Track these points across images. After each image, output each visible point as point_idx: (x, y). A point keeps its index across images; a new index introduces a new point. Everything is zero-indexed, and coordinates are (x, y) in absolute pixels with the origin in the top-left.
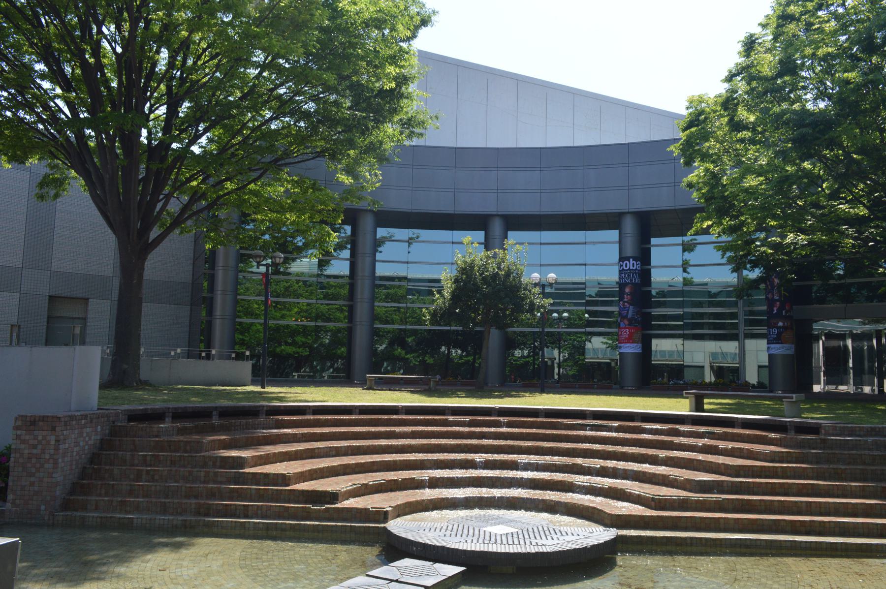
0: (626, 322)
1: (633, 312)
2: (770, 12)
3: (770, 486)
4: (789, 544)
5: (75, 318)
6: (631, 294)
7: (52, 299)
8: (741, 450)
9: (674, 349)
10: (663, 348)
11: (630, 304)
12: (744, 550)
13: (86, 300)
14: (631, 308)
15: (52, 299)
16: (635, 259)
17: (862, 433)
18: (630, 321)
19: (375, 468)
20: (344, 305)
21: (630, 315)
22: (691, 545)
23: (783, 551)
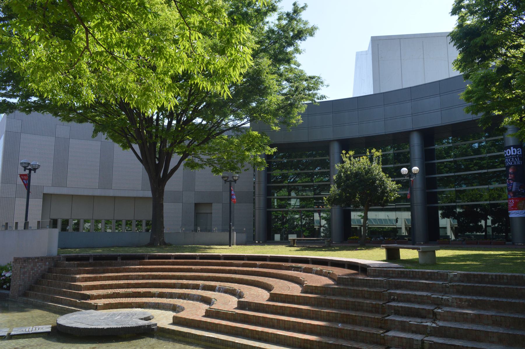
0: (512, 195)
1: (516, 186)
2: (300, 68)
3: (274, 308)
4: (231, 344)
5: (207, 213)
6: (514, 173)
7: (196, 205)
8: (209, 277)
9: (387, 218)
10: (380, 218)
11: (514, 181)
12: (181, 338)
13: (210, 204)
14: (515, 183)
15: (196, 205)
16: (514, 147)
17: (394, 275)
18: (515, 193)
19: (148, 286)
20: (512, 187)
21: (514, 190)
22: (189, 337)
23: (188, 340)
